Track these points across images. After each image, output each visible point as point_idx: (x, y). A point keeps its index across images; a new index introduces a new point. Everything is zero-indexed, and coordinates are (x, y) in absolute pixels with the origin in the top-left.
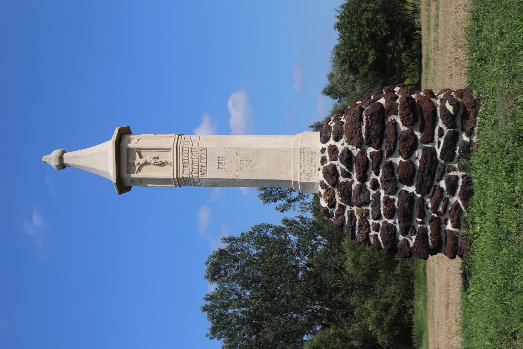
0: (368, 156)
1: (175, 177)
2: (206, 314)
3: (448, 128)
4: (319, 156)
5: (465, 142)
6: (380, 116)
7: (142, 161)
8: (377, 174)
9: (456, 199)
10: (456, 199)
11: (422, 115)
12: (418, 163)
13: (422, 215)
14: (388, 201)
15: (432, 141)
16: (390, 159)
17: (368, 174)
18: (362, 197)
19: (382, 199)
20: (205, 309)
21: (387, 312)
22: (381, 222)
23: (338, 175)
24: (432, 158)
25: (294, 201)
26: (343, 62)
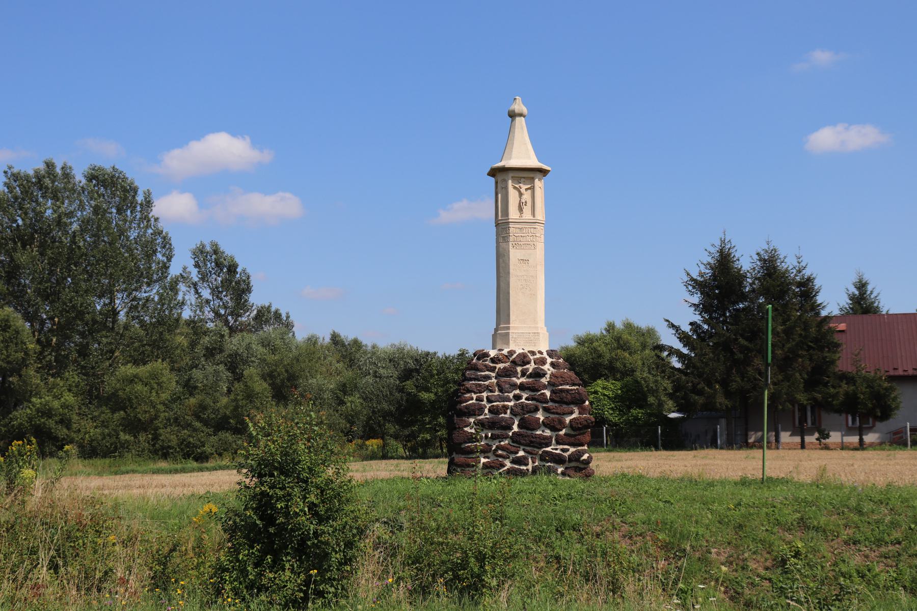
0: (543, 391)
1: (510, 220)
2: (42, 167)
3: (569, 456)
4: (535, 349)
5: (557, 470)
6: (578, 400)
7: (523, 190)
8: (527, 399)
9: (508, 464)
10: (508, 464)
11: (579, 435)
12: (539, 432)
13: (494, 437)
14: (505, 408)
15: (558, 443)
16: (541, 410)
17: (526, 391)
18: (507, 386)
19: (506, 403)
20: (50, 165)
21: (60, 422)
22: (485, 403)
23: (523, 366)
24: (544, 444)
25: (197, 292)
26: (416, 360)
